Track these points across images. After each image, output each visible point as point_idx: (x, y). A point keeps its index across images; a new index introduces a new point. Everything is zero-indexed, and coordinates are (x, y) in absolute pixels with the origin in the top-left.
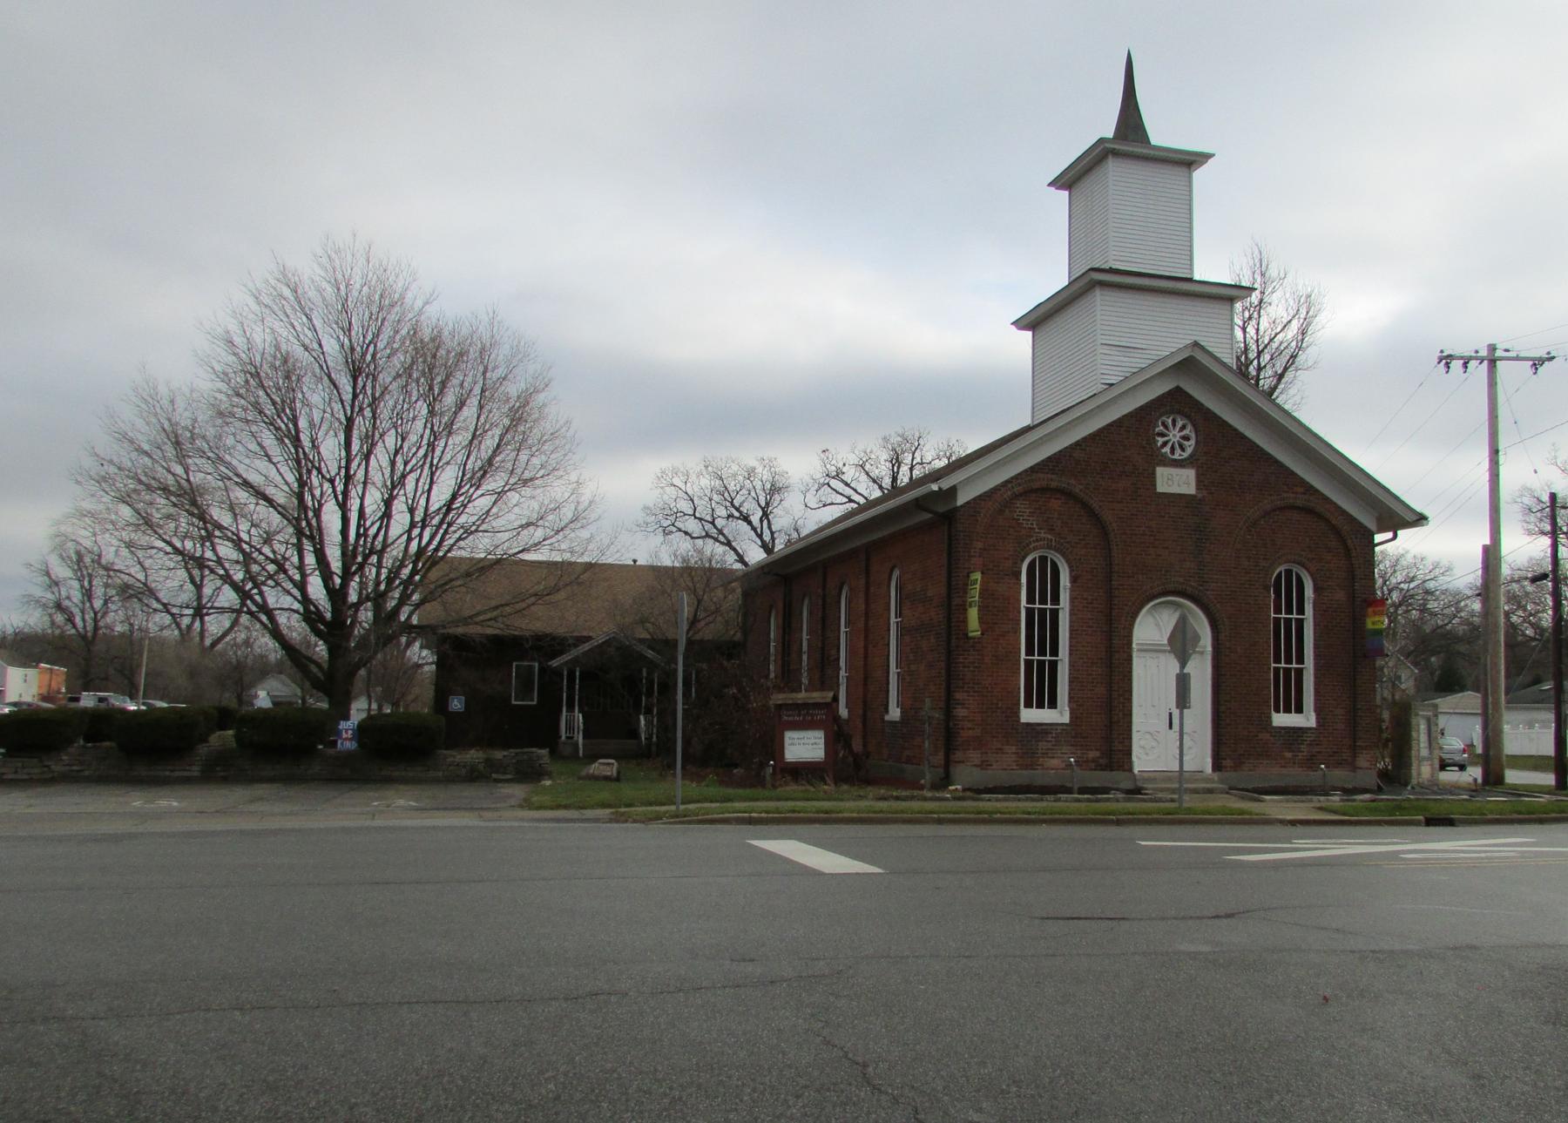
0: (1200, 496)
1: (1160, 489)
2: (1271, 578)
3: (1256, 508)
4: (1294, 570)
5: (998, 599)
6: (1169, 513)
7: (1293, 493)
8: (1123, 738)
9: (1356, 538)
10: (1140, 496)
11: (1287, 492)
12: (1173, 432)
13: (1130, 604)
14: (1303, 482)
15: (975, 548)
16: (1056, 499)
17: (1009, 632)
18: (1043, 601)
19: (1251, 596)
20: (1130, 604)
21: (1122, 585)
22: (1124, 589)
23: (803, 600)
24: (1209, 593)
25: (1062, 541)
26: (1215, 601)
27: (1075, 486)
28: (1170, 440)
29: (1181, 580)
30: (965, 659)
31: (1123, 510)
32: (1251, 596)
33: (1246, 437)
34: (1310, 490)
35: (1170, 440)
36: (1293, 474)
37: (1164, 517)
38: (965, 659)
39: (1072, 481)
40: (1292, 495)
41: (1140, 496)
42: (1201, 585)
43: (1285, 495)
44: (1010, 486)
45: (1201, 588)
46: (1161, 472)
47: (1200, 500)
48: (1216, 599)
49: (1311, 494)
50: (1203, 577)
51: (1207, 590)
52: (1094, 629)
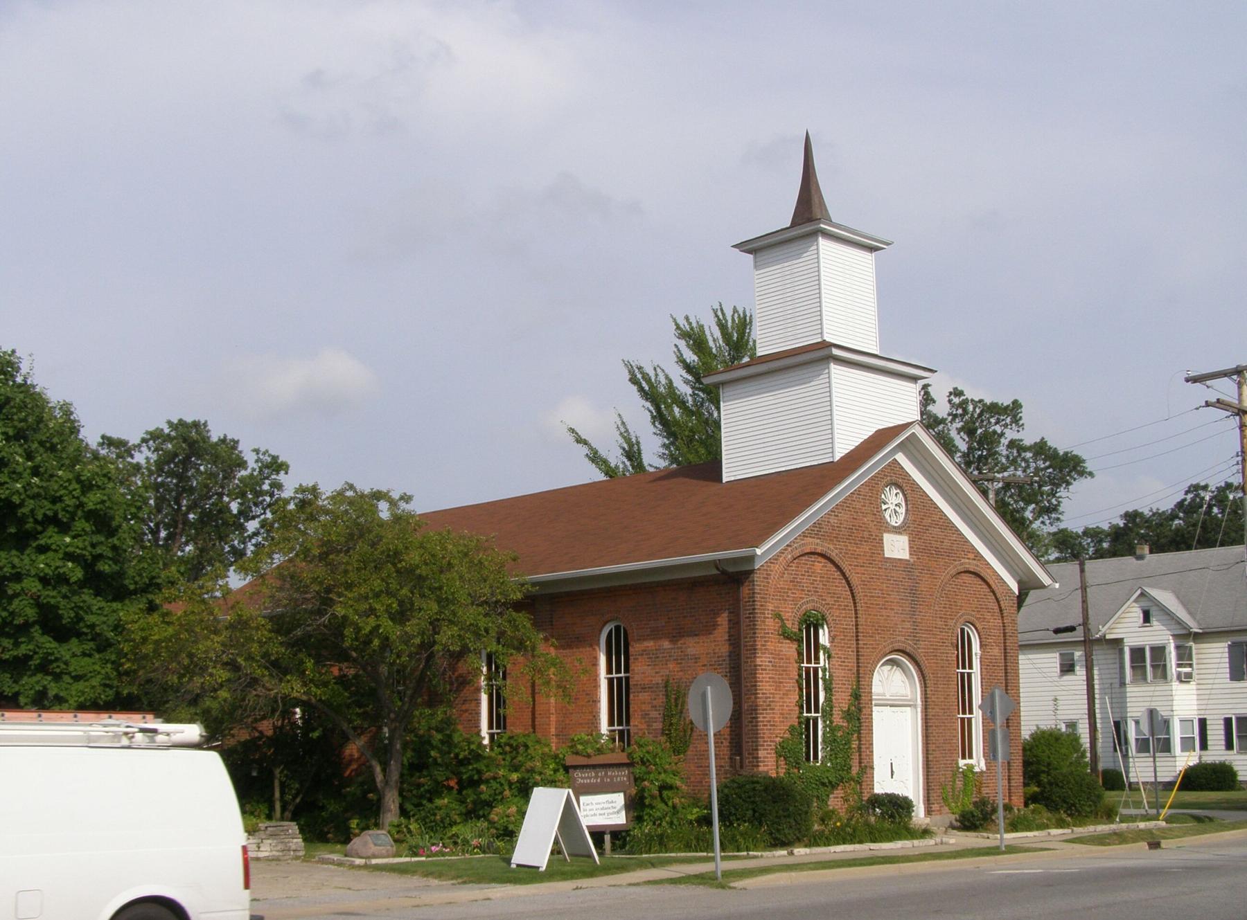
4: (966, 628)
5: (783, 659)
17: (790, 691)
21: (866, 644)
32: (943, 653)
33: (938, 507)
34: (978, 556)
39: (831, 547)
40: (967, 561)
42: (915, 644)
43: (963, 560)
44: (790, 549)
51: (919, 648)
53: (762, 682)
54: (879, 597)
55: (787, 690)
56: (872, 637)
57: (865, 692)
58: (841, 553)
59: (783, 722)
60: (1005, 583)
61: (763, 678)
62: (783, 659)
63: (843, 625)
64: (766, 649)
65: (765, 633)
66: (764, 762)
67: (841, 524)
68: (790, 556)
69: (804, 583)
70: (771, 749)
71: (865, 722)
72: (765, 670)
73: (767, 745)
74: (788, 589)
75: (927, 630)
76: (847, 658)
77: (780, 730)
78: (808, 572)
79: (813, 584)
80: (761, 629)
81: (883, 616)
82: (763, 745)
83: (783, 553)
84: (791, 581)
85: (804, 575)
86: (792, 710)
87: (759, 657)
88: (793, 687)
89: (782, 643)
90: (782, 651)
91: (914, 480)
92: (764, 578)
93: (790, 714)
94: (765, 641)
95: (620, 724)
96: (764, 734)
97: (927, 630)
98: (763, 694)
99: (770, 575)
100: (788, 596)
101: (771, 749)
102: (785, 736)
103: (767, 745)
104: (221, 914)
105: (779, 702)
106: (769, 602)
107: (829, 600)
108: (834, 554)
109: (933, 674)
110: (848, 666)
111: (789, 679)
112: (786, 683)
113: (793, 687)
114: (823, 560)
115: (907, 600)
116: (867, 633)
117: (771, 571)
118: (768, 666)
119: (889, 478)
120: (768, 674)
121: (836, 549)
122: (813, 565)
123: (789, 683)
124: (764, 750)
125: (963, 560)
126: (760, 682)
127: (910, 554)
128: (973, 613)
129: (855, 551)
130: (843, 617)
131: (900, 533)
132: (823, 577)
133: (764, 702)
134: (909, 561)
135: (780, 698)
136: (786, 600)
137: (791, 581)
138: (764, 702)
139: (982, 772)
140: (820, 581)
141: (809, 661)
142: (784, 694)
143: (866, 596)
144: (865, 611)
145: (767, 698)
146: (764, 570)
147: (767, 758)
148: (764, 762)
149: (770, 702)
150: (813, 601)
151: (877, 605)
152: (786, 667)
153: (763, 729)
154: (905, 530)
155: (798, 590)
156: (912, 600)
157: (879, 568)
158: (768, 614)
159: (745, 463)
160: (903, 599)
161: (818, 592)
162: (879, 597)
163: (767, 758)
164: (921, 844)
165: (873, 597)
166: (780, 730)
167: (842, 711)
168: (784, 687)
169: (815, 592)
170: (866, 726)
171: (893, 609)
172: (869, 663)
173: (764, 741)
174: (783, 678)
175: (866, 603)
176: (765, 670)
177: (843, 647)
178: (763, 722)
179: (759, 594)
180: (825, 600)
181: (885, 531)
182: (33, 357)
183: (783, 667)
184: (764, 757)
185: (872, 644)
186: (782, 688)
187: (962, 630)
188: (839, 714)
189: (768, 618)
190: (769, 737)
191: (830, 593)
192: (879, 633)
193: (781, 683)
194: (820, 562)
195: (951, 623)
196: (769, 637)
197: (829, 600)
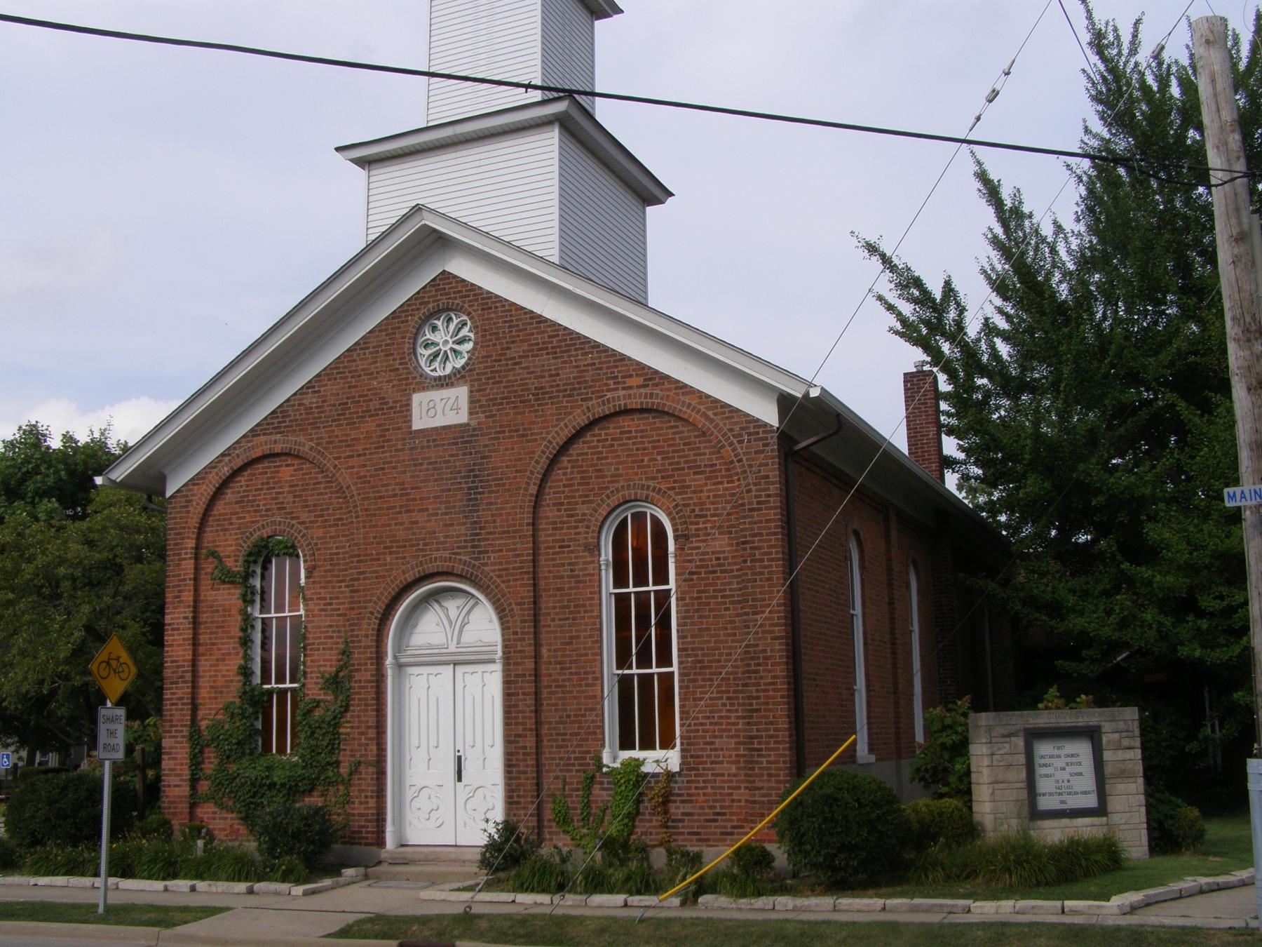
0: (474, 423)
1: (417, 425)
2: (305, 556)
3: (562, 424)
4: (648, 512)
5: (218, 611)
6: (428, 458)
7: (623, 389)
8: (366, 797)
9: (741, 442)
10: (388, 441)
11: (616, 389)
12: (451, 341)
13: (375, 598)
14: (641, 368)
15: (186, 548)
16: (287, 466)
17: (229, 654)
18: (641, 580)
19: (563, 565)
20: (375, 598)
22: (364, 579)
23: (907, 573)
24: (486, 569)
25: (294, 522)
26: (498, 580)
27: (304, 444)
28: (453, 342)
29: (446, 554)
30: (173, 694)
31: (365, 466)
32: (563, 565)
33: (546, 320)
35: (446, 352)
36: (623, 358)
37: (421, 464)
38: (173, 694)
39: (302, 439)
40: (622, 393)
41: (388, 441)
42: (476, 559)
44: (227, 459)
45: (476, 563)
46: (419, 399)
47: (474, 430)
48: (499, 576)
49: (657, 385)
50: (479, 546)
51: (485, 564)
52: (335, 640)
53: (172, 645)
54: (395, 495)
55: (223, 654)
56: (379, 559)
57: (360, 647)
58: (318, 444)
59: (216, 698)
60: (738, 411)
61: (173, 640)
62: (218, 611)
63: (331, 548)
64: (180, 602)
65: (180, 581)
66: (170, 753)
67: (324, 401)
68: (226, 469)
69: (260, 500)
70: (183, 737)
71: (359, 693)
72: (178, 629)
73: (176, 731)
74: (231, 514)
75: (504, 532)
76: (337, 598)
77: (210, 709)
78: (268, 483)
79: (275, 498)
80: (173, 576)
81: (401, 524)
82: (169, 732)
83: (214, 467)
84: (237, 503)
85: (262, 489)
86: (232, 681)
87: (169, 614)
88: (234, 648)
89: (219, 589)
90: (217, 600)
91: (488, 292)
92: (183, 507)
93: (227, 687)
94: (179, 591)
95: (644, 661)
96: (171, 715)
97: (504, 532)
98: (172, 662)
99: (191, 501)
100: (231, 524)
101: (183, 737)
102: (219, 717)
103: (176, 731)
104: (432, 849)
105: (210, 671)
106: (188, 538)
107: (304, 516)
108: (306, 449)
109: (517, 604)
110: (339, 609)
111: (228, 638)
112: (223, 644)
113: (234, 648)
114: (296, 462)
115: (460, 489)
116: (366, 555)
117: (192, 495)
118: (181, 623)
119: (430, 306)
120: (180, 634)
121: (311, 440)
122: (278, 472)
123: (228, 643)
124: (170, 737)
125: (609, 395)
126: (169, 646)
127: (471, 413)
128: (651, 483)
129: (347, 435)
130: (332, 537)
131: (452, 385)
132: (297, 485)
133: (174, 672)
134: (468, 424)
135: (211, 666)
136: (227, 530)
137: (237, 503)
138: (174, 672)
139: (670, 776)
140: (289, 492)
141: (641, 580)
142: (217, 660)
143: (368, 498)
144: (364, 521)
145: (178, 667)
146: (182, 496)
147: (176, 748)
148: (170, 753)
149: (183, 672)
150: (274, 523)
151: (389, 508)
152: (223, 622)
153: (171, 710)
154: (463, 377)
155: (249, 512)
156: (469, 488)
157: (397, 450)
158: (186, 554)
159: (626, 275)
160: (449, 490)
161: (285, 508)
162: (395, 495)
163: (176, 748)
164: (214, 889)
165: (381, 497)
166: (210, 709)
167: (323, 677)
168: (219, 649)
169: (279, 509)
170: (360, 699)
171: (427, 510)
172: (370, 601)
173: (172, 726)
174: (215, 638)
175: (367, 510)
176: (178, 629)
177: (330, 582)
178: (171, 699)
179: (172, 529)
180: (297, 518)
181: (414, 391)
182: (856, 234)
183: (217, 622)
184: (171, 748)
185: (376, 572)
186: (216, 652)
187: (639, 518)
188: (317, 683)
189: (185, 559)
190: (179, 720)
191: (307, 506)
192: (390, 553)
193: (213, 644)
194: (293, 465)
195: (582, 509)
196: (185, 585)
197: (304, 516)
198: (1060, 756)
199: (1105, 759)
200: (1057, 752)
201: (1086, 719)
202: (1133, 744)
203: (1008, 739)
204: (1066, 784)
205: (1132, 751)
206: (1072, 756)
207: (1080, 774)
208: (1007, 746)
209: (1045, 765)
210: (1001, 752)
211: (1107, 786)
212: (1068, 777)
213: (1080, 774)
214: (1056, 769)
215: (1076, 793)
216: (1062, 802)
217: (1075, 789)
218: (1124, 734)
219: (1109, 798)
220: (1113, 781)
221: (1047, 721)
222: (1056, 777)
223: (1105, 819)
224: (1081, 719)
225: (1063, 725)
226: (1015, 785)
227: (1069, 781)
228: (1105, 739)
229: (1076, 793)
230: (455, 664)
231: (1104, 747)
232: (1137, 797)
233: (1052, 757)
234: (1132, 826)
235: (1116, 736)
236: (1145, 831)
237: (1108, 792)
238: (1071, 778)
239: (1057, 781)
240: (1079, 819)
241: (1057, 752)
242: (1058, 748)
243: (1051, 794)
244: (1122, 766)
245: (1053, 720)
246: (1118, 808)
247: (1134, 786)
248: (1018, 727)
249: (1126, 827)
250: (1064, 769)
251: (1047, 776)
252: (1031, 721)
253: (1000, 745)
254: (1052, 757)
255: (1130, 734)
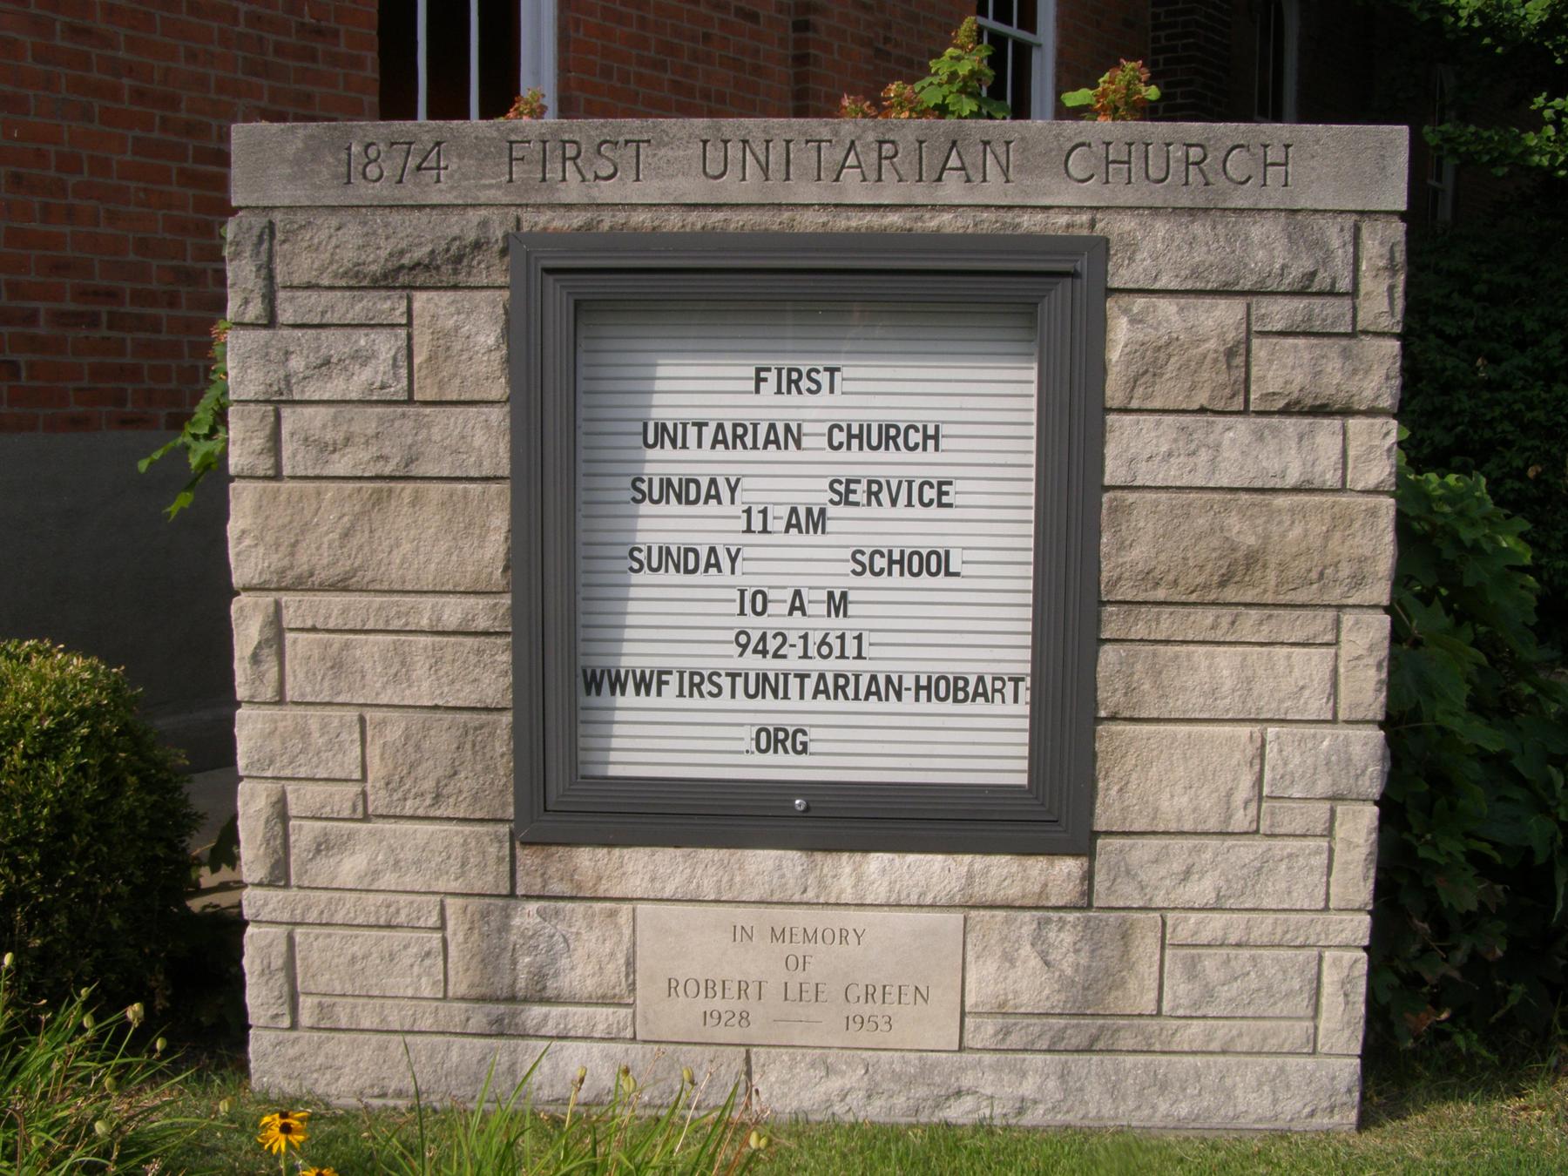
1: (241, 134)
198: (794, 436)
199: (1113, 472)
200: (770, 406)
201: (994, 190)
202: (1334, 378)
203: (389, 306)
204: (818, 621)
205: (1326, 433)
206: (889, 436)
207: (936, 563)
208: (386, 346)
209: (682, 491)
210: (335, 388)
211: (1109, 656)
212: (841, 577)
213: (936, 563)
214: (756, 521)
215: (885, 687)
216: (774, 739)
217: (879, 662)
218: (1278, 312)
219: (1109, 737)
220: (1166, 624)
221: (693, 188)
222: (749, 576)
223: (1068, 867)
224: (952, 189)
225: (810, 221)
226: (425, 611)
227: (838, 603)
228: (1121, 333)
229: (885, 687)
230: (1257, 832)
231: (1114, 391)
232: (1327, 738)
233: (733, 436)
234: (1264, 926)
235: (1224, 316)
236: (1359, 962)
237: (1109, 696)
238: (863, 589)
239: (758, 602)
240: (876, 862)
241: (770, 406)
242: (790, 382)
243: (695, 682)
244: (1242, 530)
245: (741, 186)
246: (1174, 805)
247: (1314, 664)
248: (465, 226)
249: (1215, 924)
250: (816, 521)
251: (682, 560)
252: (572, 191)
253: (335, 344)
254: (733, 436)
255: (1331, 312)
